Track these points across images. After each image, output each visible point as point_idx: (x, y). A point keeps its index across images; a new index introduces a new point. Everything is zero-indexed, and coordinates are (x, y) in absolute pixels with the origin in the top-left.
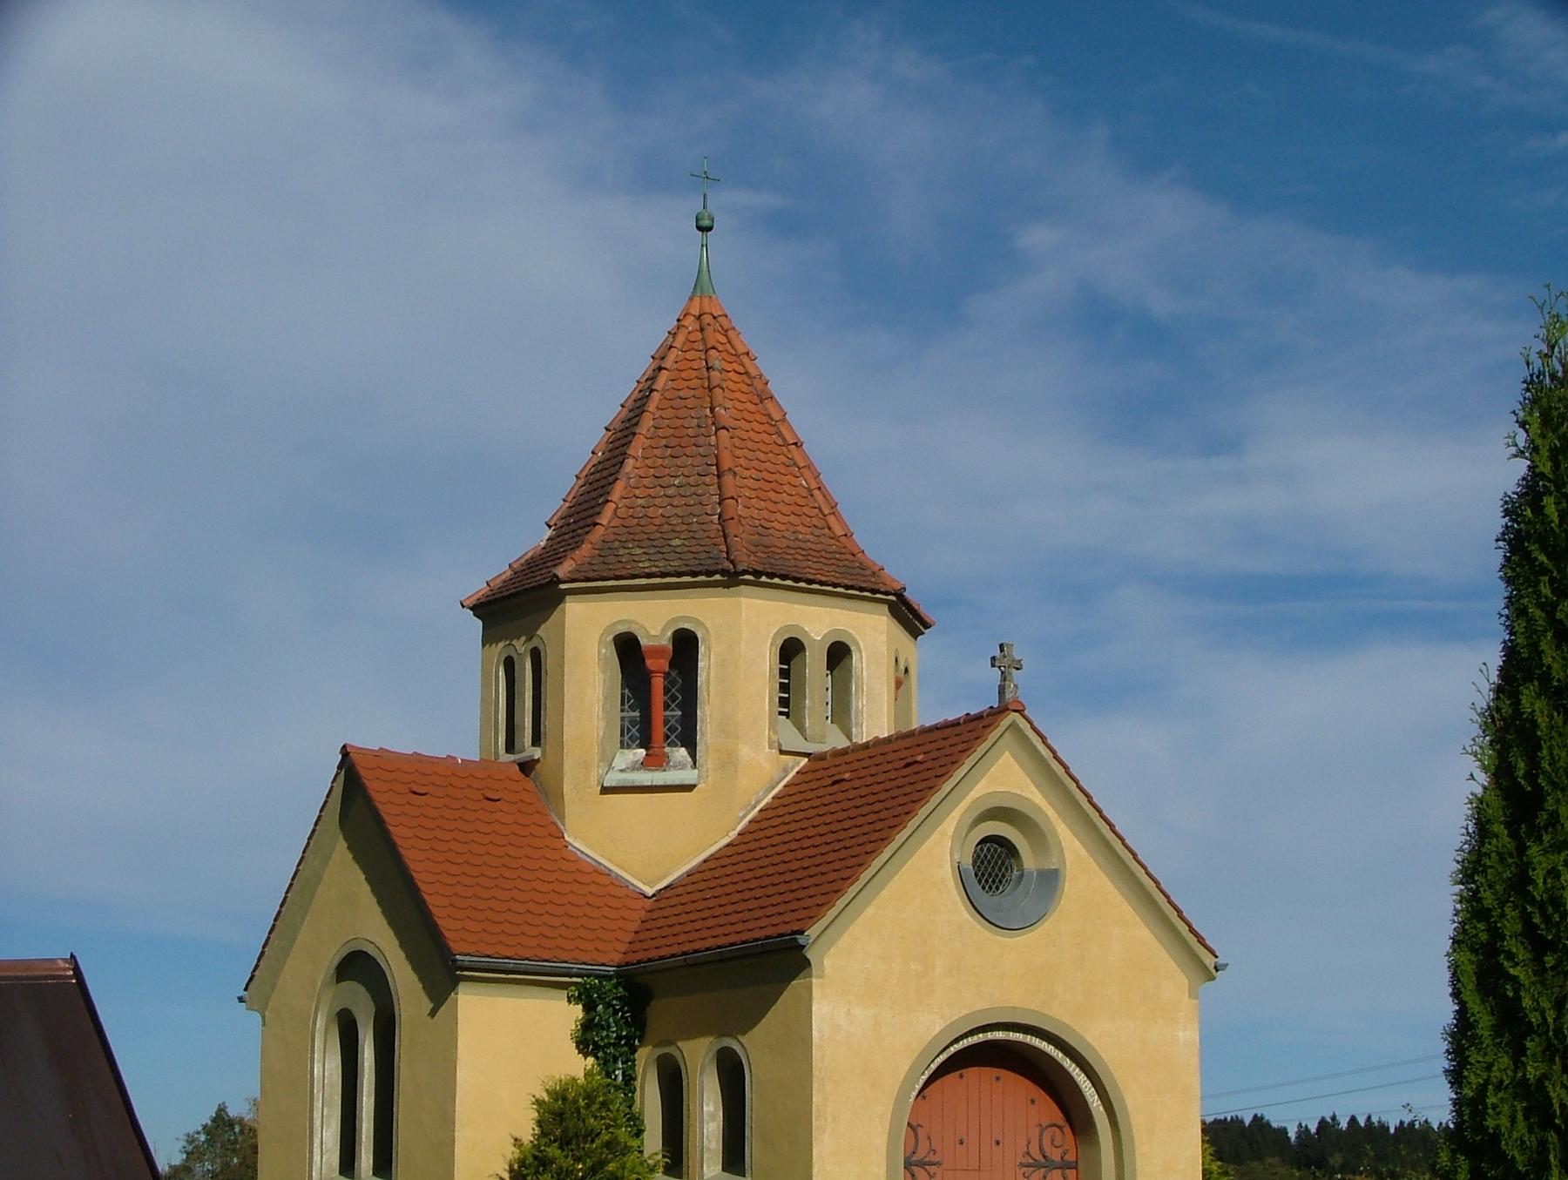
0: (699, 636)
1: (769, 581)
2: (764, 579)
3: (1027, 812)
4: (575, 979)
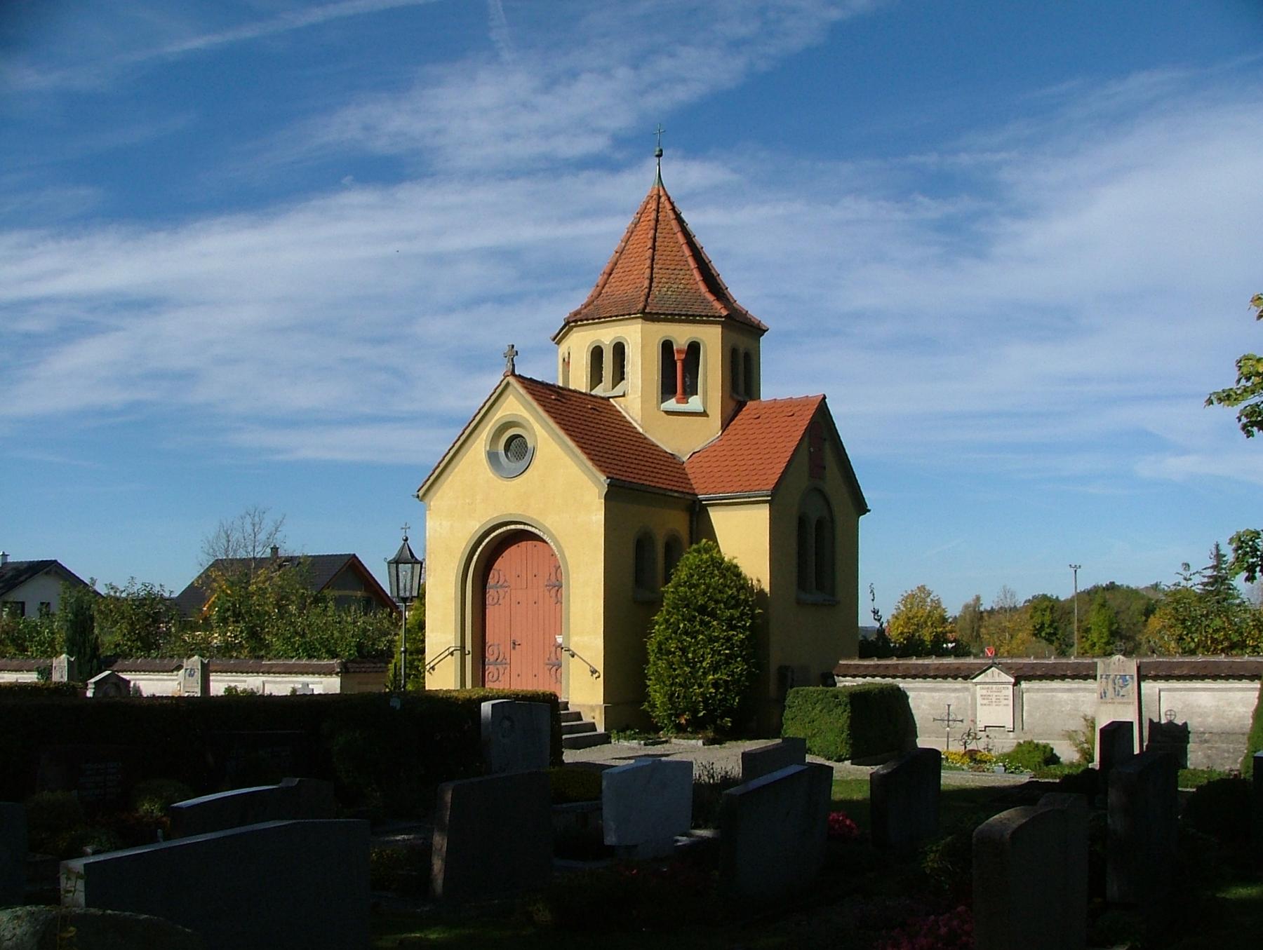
2: (579, 323)
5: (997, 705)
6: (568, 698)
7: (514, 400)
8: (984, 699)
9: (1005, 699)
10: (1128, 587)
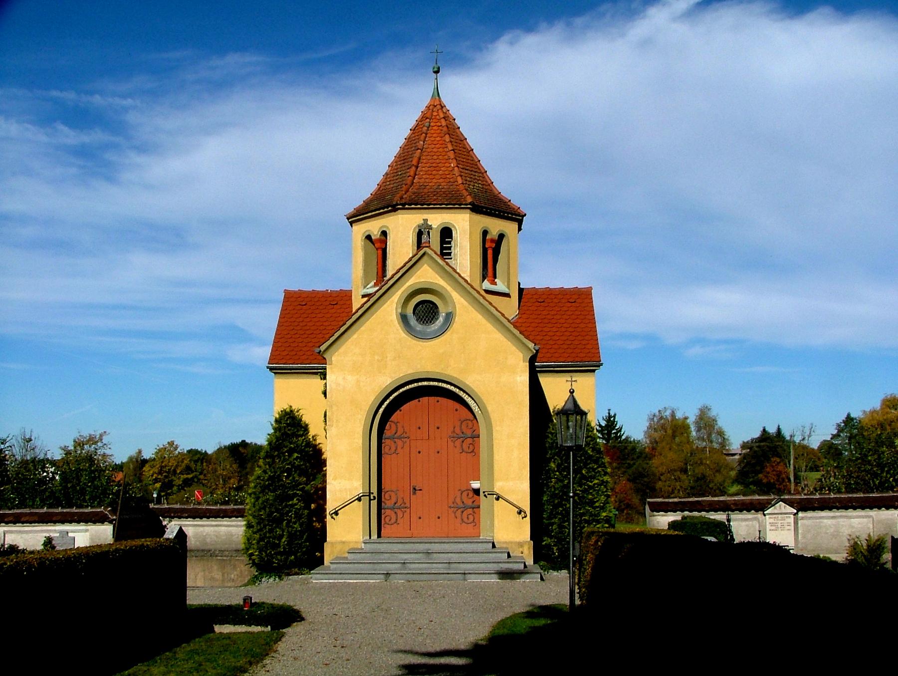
1: (422, 207)
2: (407, 206)
3: (437, 289)
4: (319, 371)
5: (782, 530)
6: (493, 537)
7: (428, 268)
8: (772, 526)
9: (788, 525)
10: (255, 444)
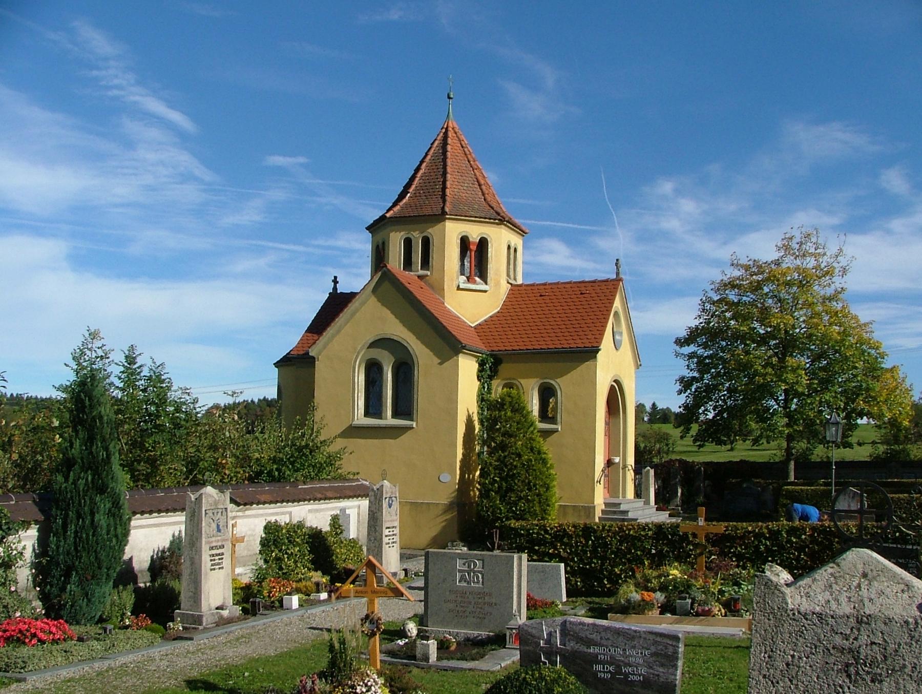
0: (489, 240)
